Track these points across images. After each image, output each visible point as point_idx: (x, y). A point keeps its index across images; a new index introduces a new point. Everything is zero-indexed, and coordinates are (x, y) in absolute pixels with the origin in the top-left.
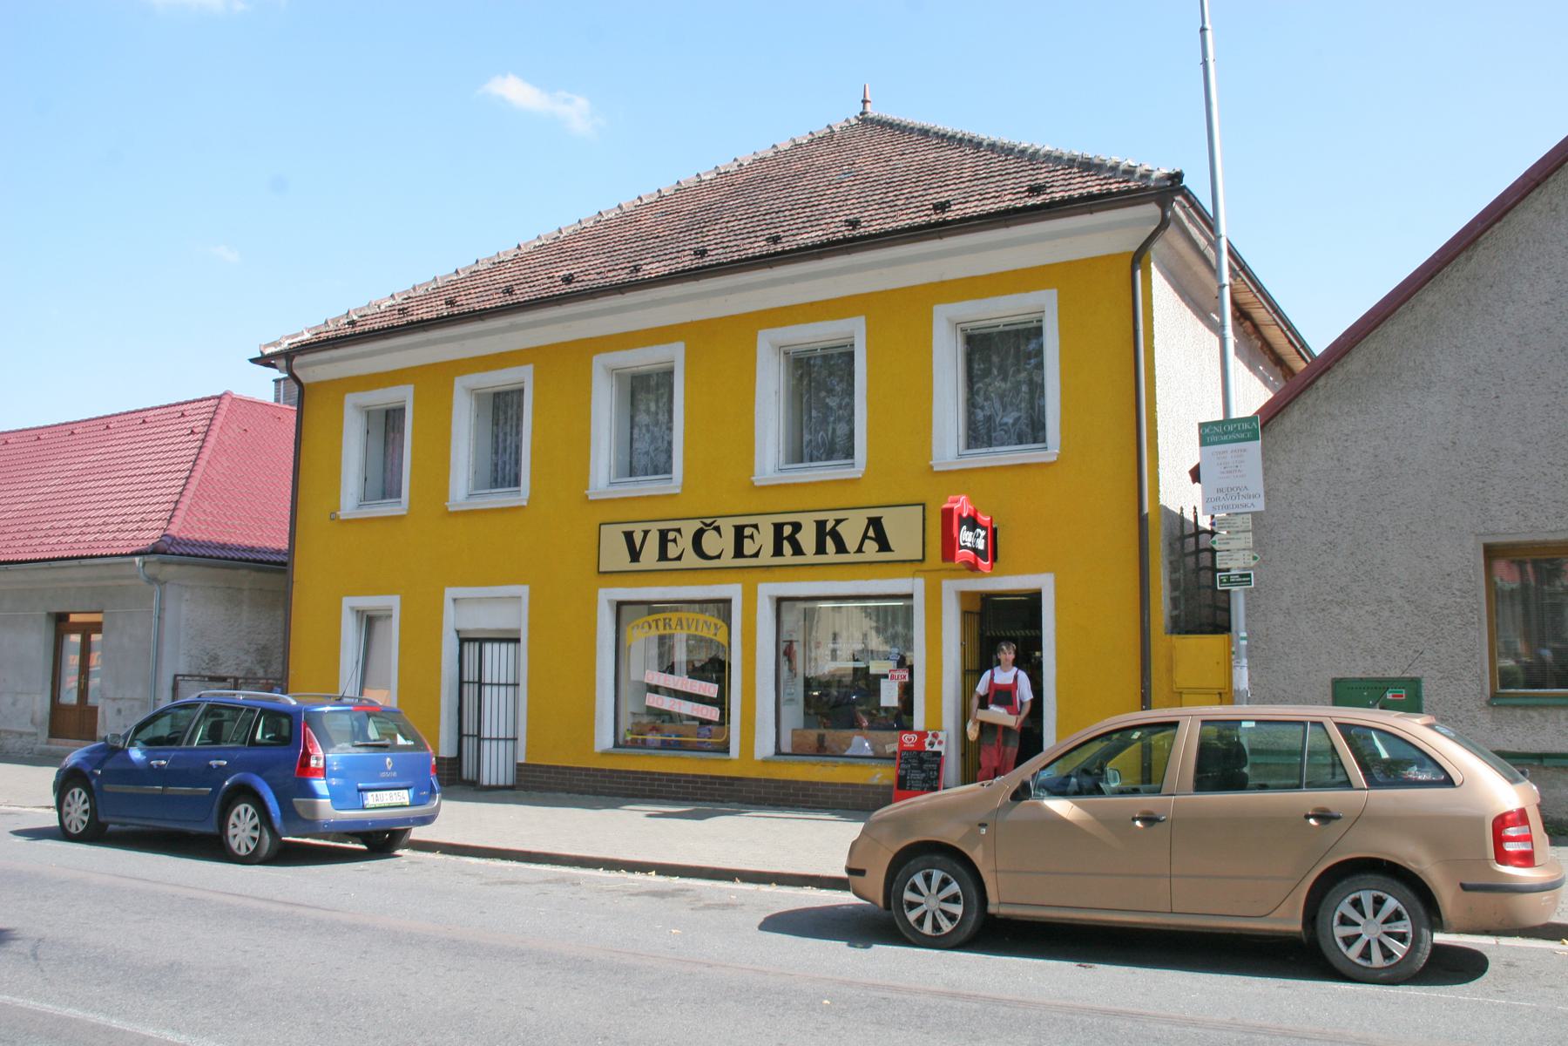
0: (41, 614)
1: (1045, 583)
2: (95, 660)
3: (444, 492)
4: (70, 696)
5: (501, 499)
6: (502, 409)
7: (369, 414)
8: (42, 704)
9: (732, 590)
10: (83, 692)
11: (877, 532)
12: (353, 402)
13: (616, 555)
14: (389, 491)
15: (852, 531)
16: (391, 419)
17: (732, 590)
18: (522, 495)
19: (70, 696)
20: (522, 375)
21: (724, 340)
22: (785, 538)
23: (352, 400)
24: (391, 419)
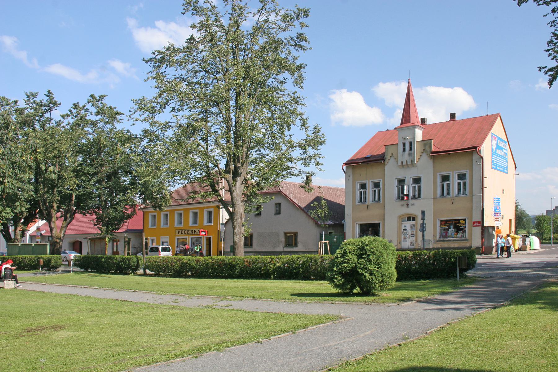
0: (250, 231)
1: (211, 236)
2: (119, 246)
3: (203, 223)
4: (115, 250)
5: (195, 225)
6: (195, 214)
7: (152, 216)
8: (111, 252)
9: (187, 237)
10: (117, 250)
11: (195, 231)
12: (150, 214)
13: (177, 233)
14: (181, 223)
15: (197, 231)
16: (181, 215)
17: (187, 237)
18: (198, 225)
19: (115, 250)
20: (182, 212)
21: (187, 210)
22: (192, 232)
23: (176, 212)
24: (181, 214)
